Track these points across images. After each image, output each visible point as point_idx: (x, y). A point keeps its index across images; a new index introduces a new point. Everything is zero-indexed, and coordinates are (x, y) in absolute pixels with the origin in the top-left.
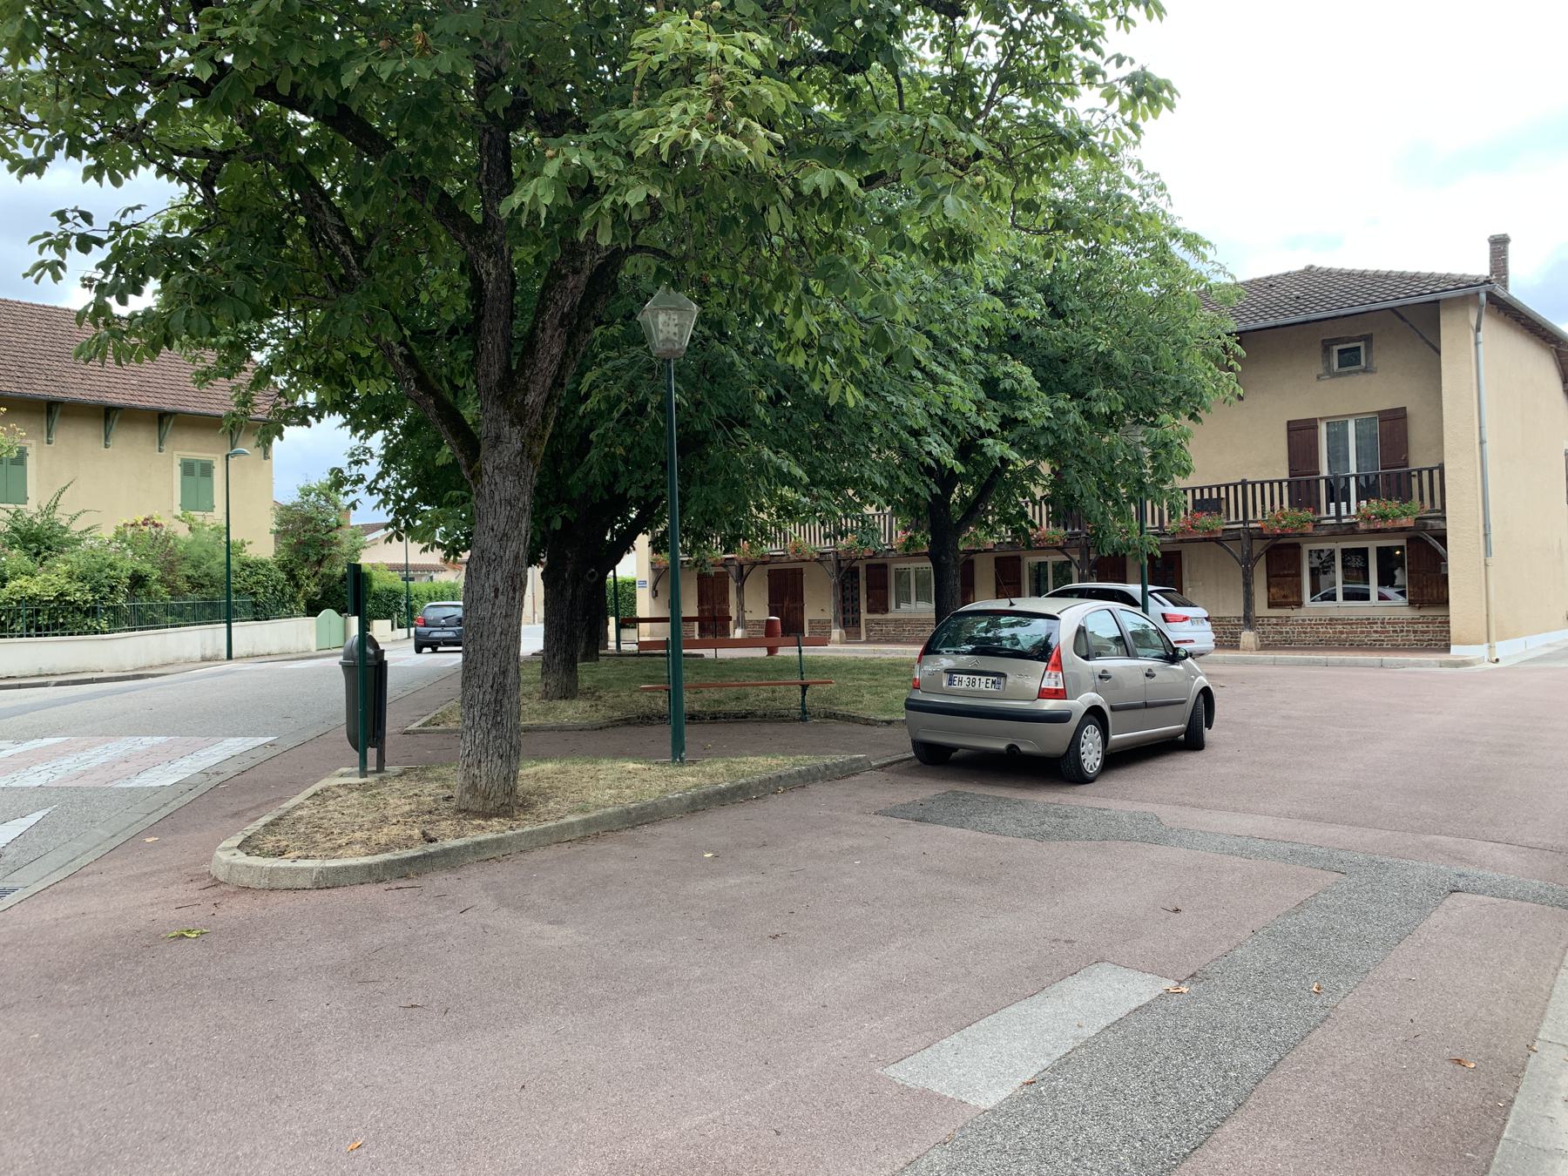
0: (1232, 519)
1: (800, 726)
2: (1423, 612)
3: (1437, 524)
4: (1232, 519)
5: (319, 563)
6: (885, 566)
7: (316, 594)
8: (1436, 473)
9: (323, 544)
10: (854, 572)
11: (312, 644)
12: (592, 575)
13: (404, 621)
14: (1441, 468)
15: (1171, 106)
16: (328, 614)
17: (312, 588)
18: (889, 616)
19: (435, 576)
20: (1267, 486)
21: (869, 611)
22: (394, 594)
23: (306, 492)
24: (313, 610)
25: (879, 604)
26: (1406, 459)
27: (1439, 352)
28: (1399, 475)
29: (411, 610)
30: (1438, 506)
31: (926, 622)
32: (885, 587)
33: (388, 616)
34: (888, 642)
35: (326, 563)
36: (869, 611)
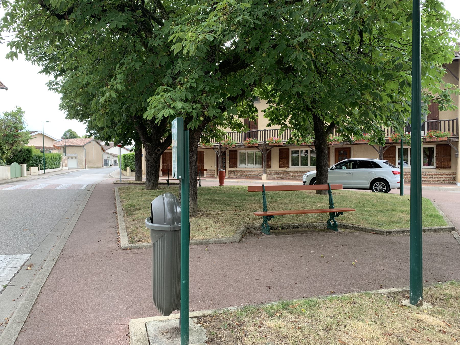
0: (261, 141)
1: (332, 236)
2: (441, 171)
3: (455, 140)
4: (261, 141)
5: (12, 144)
6: (236, 151)
7: (10, 156)
8: (455, 122)
9: (15, 136)
10: (224, 153)
11: (9, 176)
12: (159, 150)
13: (43, 167)
14: (457, 120)
15: (60, 109)
16: (15, 164)
17: (9, 154)
18: (237, 169)
19: (51, 151)
20: (274, 131)
21: (230, 167)
22: (39, 157)
23: (7, 115)
24: (9, 163)
25: (234, 164)
26: (438, 117)
27: (458, 80)
28: (436, 122)
29: (45, 163)
30: (455, 133)
31: (423, 184)
32: (236, 159)
33: (37, 165)
34: (237, 178)
35: (15, 144)
36: (230, 167)
